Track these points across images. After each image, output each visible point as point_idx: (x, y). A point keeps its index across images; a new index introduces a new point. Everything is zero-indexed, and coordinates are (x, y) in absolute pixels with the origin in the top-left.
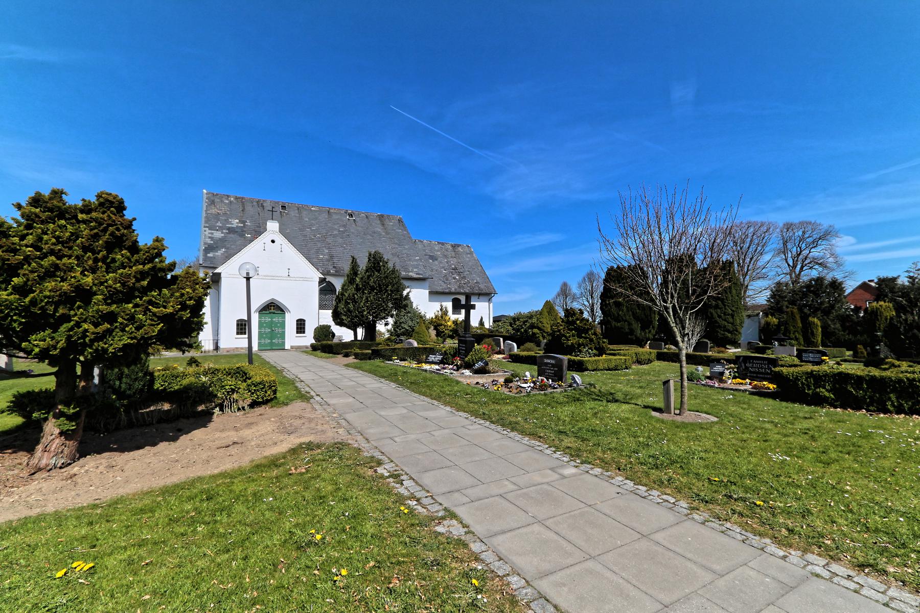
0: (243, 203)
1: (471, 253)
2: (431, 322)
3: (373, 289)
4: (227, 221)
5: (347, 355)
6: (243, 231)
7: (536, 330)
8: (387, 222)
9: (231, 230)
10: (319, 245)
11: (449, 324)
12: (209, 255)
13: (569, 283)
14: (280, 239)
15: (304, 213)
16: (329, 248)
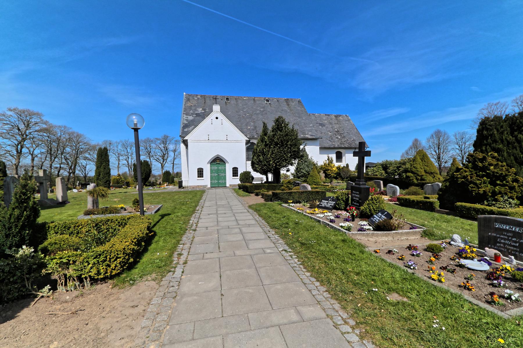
0: (205, 98)
1: (349, 120)
2: (321, 168)
3: (276, 144)
4: (196, 110)
5: (257, 195)
7: (409, 174)
9: (198, 115)
10: (248, 120)
11: (334, 169)
13: (419, 138)
14: (221, 116)
15: (240, 101)
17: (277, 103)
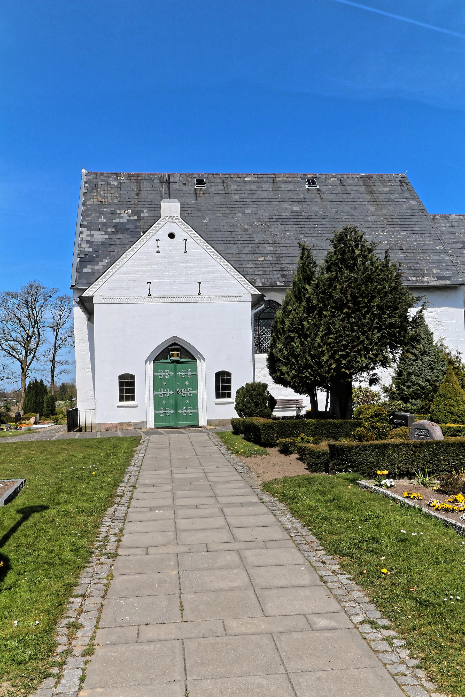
0: (138, 183)
3: (340, 306)
4: (114, 214)
5: (285, 451)
6: (136, 227)
8: (378, 187)
9: (120, 228)
10: (257, 239)
12: (85, 270)
14: (183, 230)
16: (274, 243)
17: (339, 188)
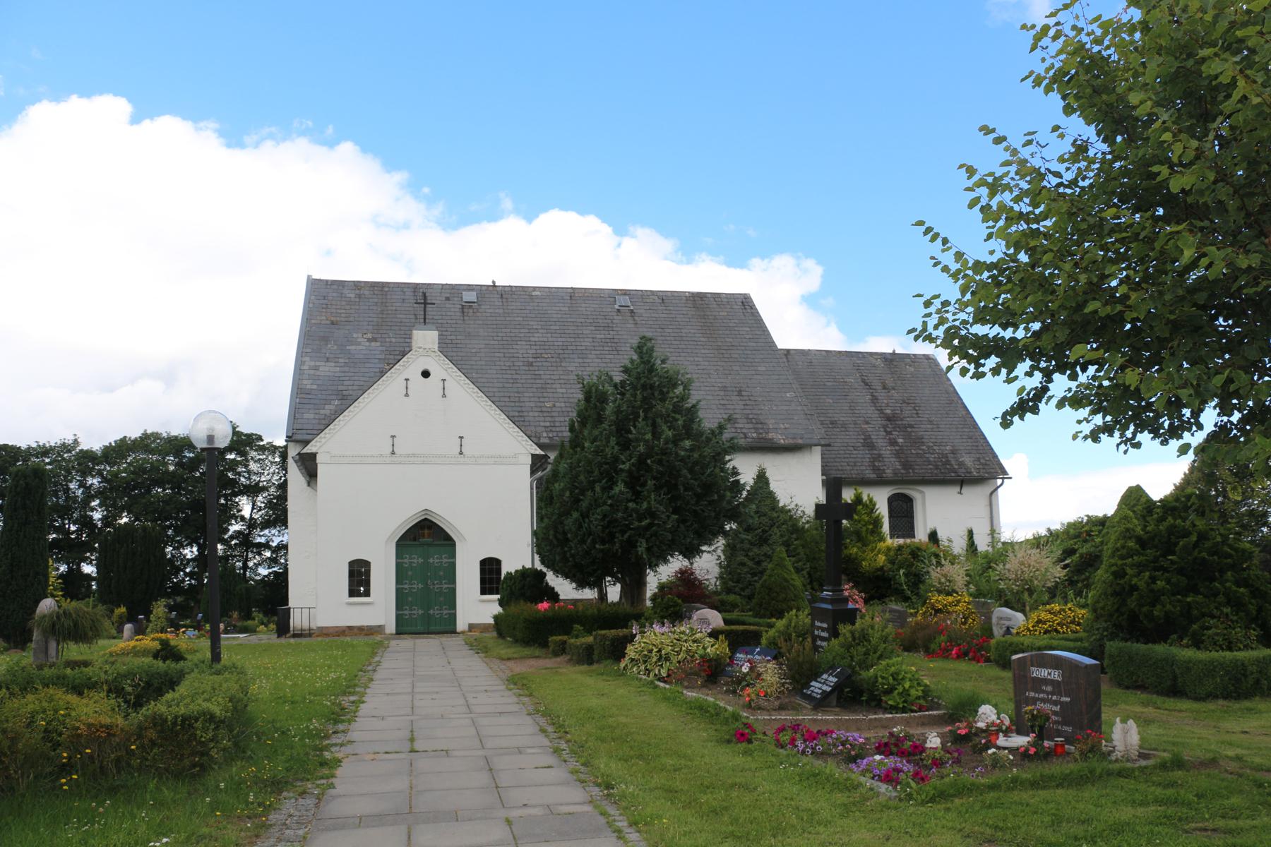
14: (441, 368)
